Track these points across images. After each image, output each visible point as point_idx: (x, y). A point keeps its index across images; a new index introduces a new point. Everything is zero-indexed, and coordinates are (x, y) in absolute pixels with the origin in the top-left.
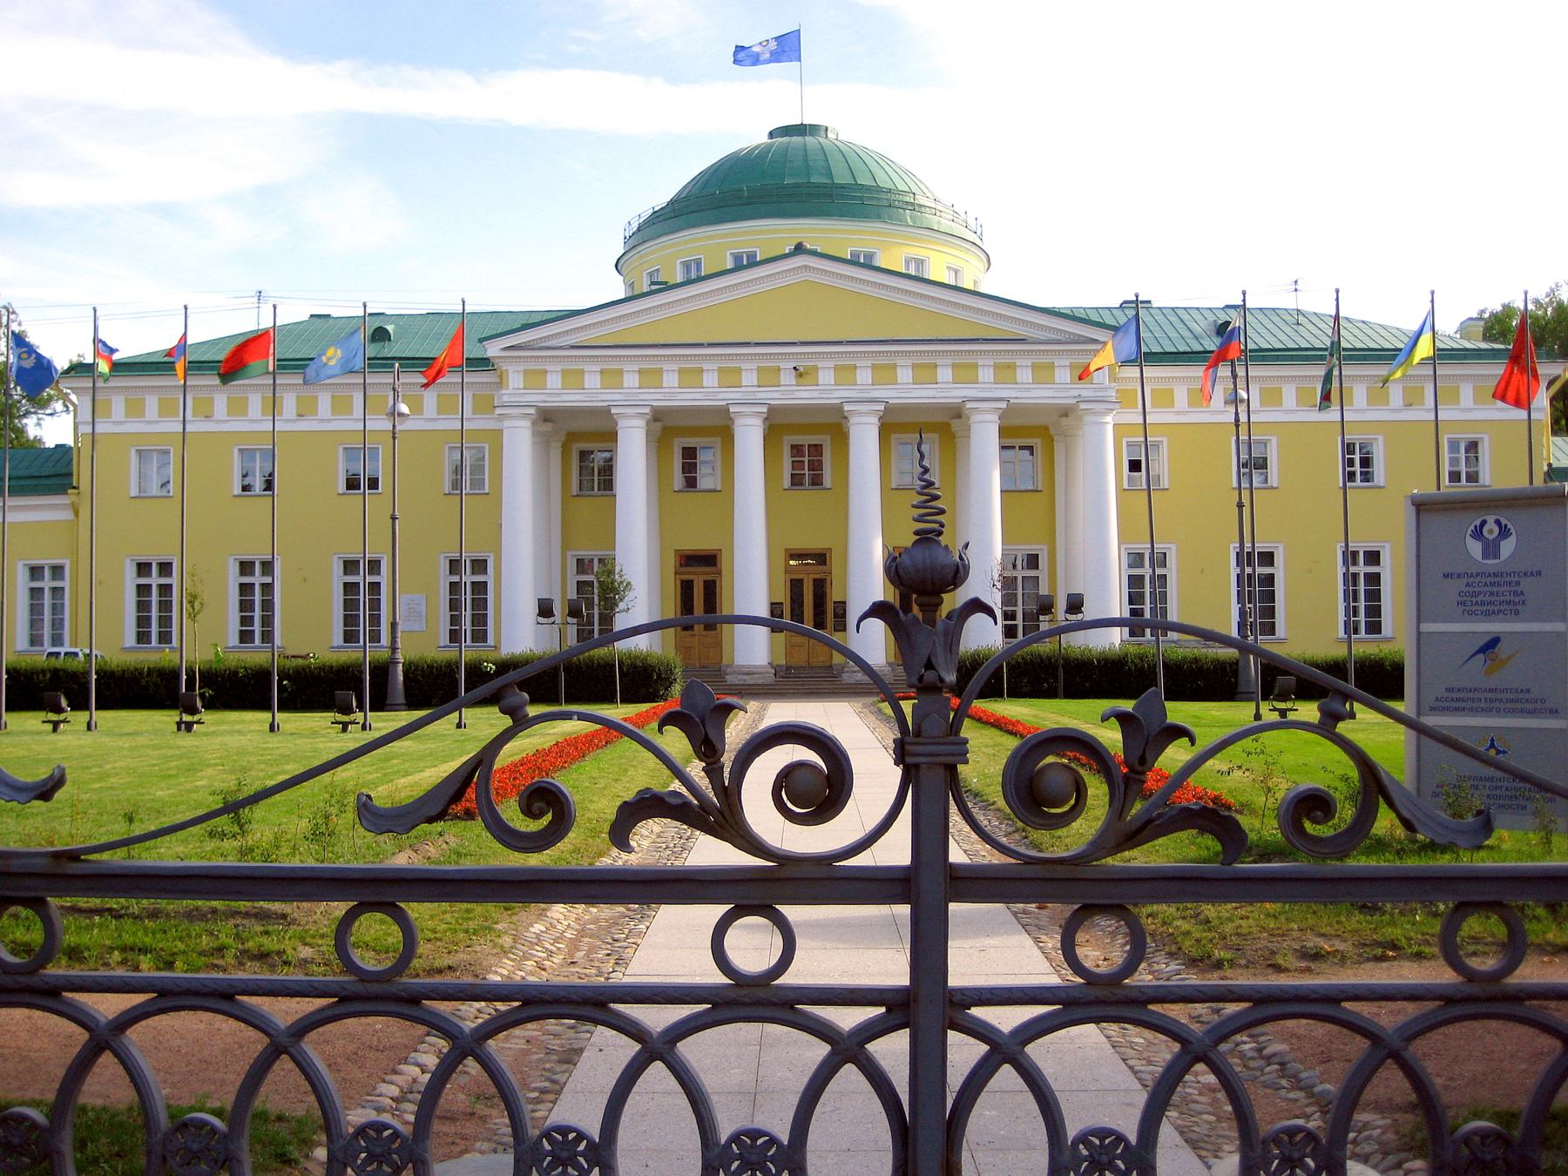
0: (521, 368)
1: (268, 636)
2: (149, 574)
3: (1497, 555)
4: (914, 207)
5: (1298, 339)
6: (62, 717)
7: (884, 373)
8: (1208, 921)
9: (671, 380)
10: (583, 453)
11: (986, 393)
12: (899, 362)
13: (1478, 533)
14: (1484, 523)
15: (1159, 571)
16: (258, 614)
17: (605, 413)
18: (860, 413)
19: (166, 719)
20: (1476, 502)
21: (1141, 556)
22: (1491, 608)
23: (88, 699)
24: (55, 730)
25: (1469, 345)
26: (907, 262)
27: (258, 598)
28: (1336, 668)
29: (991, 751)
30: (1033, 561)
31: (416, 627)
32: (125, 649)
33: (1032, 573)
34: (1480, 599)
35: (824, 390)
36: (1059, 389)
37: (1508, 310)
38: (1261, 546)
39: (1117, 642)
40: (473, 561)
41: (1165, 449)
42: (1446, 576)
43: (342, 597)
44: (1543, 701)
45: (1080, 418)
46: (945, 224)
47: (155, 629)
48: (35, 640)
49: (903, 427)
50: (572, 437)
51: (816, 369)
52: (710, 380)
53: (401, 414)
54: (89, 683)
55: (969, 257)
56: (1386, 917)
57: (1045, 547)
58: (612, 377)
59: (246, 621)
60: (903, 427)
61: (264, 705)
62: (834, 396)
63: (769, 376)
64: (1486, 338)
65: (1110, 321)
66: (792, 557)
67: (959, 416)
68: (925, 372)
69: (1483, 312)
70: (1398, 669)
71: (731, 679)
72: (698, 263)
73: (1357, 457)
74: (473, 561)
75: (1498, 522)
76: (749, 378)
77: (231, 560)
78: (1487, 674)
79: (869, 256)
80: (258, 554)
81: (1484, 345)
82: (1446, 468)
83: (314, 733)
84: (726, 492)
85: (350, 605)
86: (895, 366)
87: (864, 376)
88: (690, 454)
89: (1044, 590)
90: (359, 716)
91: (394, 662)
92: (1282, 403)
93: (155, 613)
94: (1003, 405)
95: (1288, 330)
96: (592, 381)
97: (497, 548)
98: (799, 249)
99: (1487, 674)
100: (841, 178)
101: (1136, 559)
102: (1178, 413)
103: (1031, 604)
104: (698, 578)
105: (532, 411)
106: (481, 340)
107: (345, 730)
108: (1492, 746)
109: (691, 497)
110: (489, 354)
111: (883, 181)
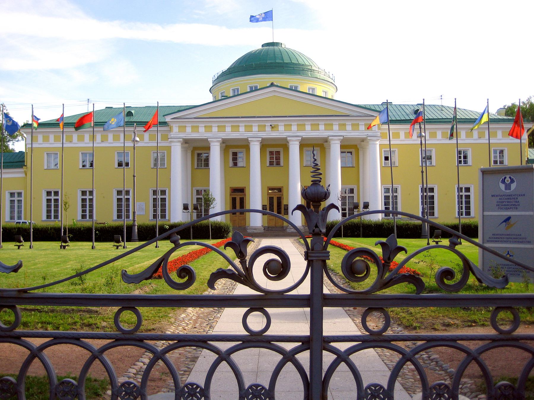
0: (178, 125)
1: (91, 216)
2: (51, 195)
3: (510, 189)
4: (311, 70)
5: (442, 115)
6: (21, 244)
7: (301, 127)
8: (411, 313)
9: (228, 129)
10: (198, 154)
11: (336, 134)
12: (306, 123)
13: (503, 181)
14: (505, 178)
15: (395, 194)
16: (88, 209)
17: (206, 140)
18: (293, 141)
19: (57, 244)
20: (503, 171)
21: (389, 189)
22: (508, 207)
23: (30, 238)
24: (19, 248)
25: (500, 117)
26: (309, 89)
27: (88, 203)
28: (455, 227)
29: (337, 255)
30: (352, 191)
31: (142, 213)
32: (43, 221)
33: (352, 195)
34: (504, 204)
35: (281, 133)
36: (361, 132)
37: (514, 105)
38: (429, 186)
39: (381, 218)
40: (161, 191)
41: (397, 153)
42: (492, 196)
43: (116, 203)
44: (525, 238)
45: (368, 142)
46: (322, 76)
47: (53, 214)
48: (12, 218)
49: (307, 145)
50: (195, 149)
51: (278, 125)
52: (242, 129)
53: (136, 141)
54: (30, 232)
55: (330, 87)
56: (472, 312)
57: (356, 186)
58: (208, 128)
59: (84, 211)
60: (307, 145)
61: (90, 240)
62: (284, 135)
63: (262, 128)
64: (506, 115)
65: (378, 109)
66: (270, 189)
67: (327, 141)
68: (315, 127)
69: (505, 106)
70: (476, 228)
71: (249, 231)
72: (238, 89)
73: (462, 156)
74: (161, 191)
75: (510, 178)
76: (255, 129)
77: (79, 191)
78: (506, 229)
79: (296, 87)
80: (88, 189)
81: (505, 118)
82: (492, 159)
83: (107, 249)
84: (247, 167)
85: (119, 206)
86: (305, 125)
87: (294, 128)
88: (235, 154)
89: (355, 201)
90: (122, 244)
91: (134, 225)
92: (437, 137)
93: (53, 209)
94: (342, 138)
95: (439, 112)
96: (202, 130)
97: (169, 186)
98: (272, 85)
99: (506, 229)
100: (286, 60)
101: (387, 190)
102: (401, 140)
103: (351, 205)
104: (238, 197)
105: (181, 140)
106: (164, 116)
107: (117, 248)
108: (508, 254)
109: (235, 169)
110: (167, 120)
111: (301, 62)
